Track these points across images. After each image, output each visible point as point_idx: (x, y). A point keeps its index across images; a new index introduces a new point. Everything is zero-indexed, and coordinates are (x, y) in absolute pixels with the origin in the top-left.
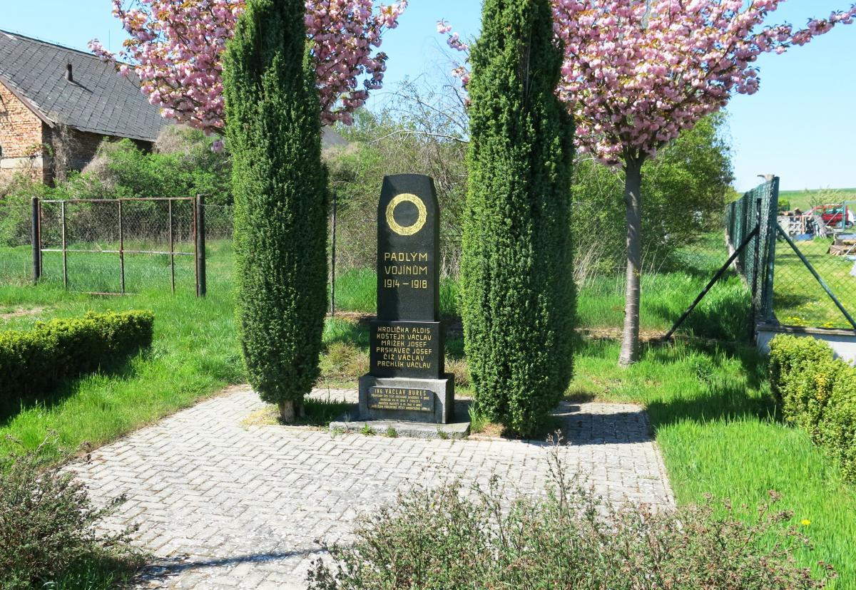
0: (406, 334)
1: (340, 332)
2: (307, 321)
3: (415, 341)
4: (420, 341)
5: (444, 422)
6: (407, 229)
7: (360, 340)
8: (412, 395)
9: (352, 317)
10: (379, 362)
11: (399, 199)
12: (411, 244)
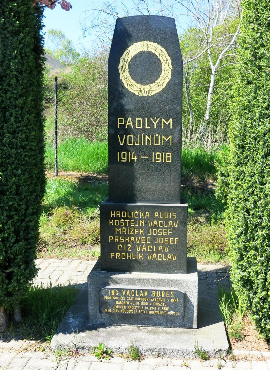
0: (146, 220)
1: (63, 192)
2: (16, 210)
3: (158, 228)
4: (164, 228)
5: (195, 326)
6: (146, 87)
7: (80, 200)
8: (156, 297)
9: (73, 177)
10: (112, 255)
11: (134, 49)
12: (146, 107)
